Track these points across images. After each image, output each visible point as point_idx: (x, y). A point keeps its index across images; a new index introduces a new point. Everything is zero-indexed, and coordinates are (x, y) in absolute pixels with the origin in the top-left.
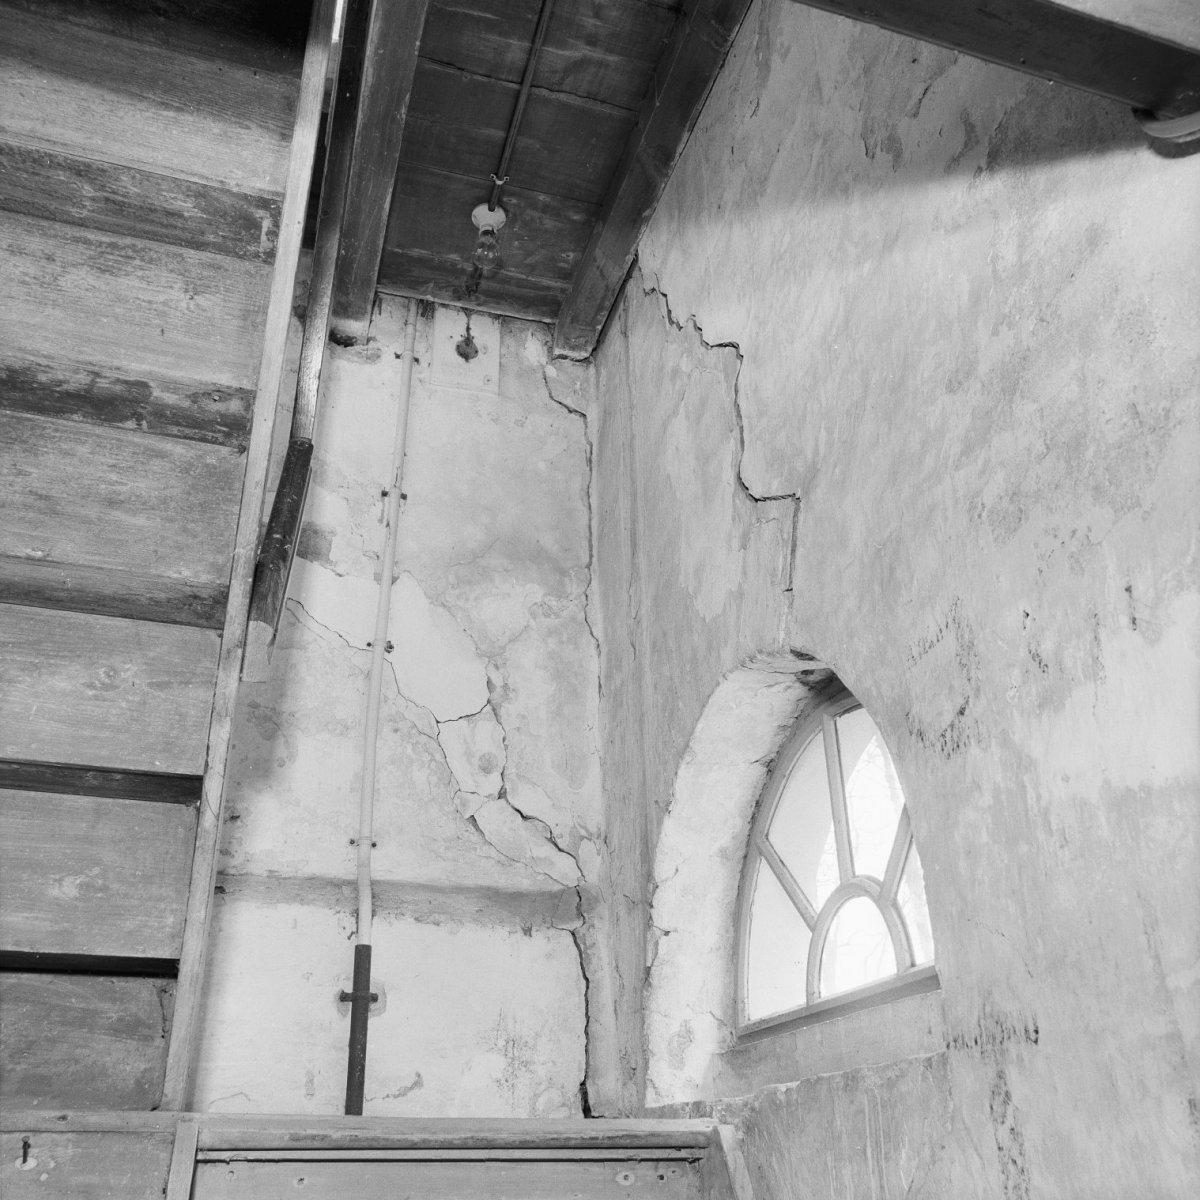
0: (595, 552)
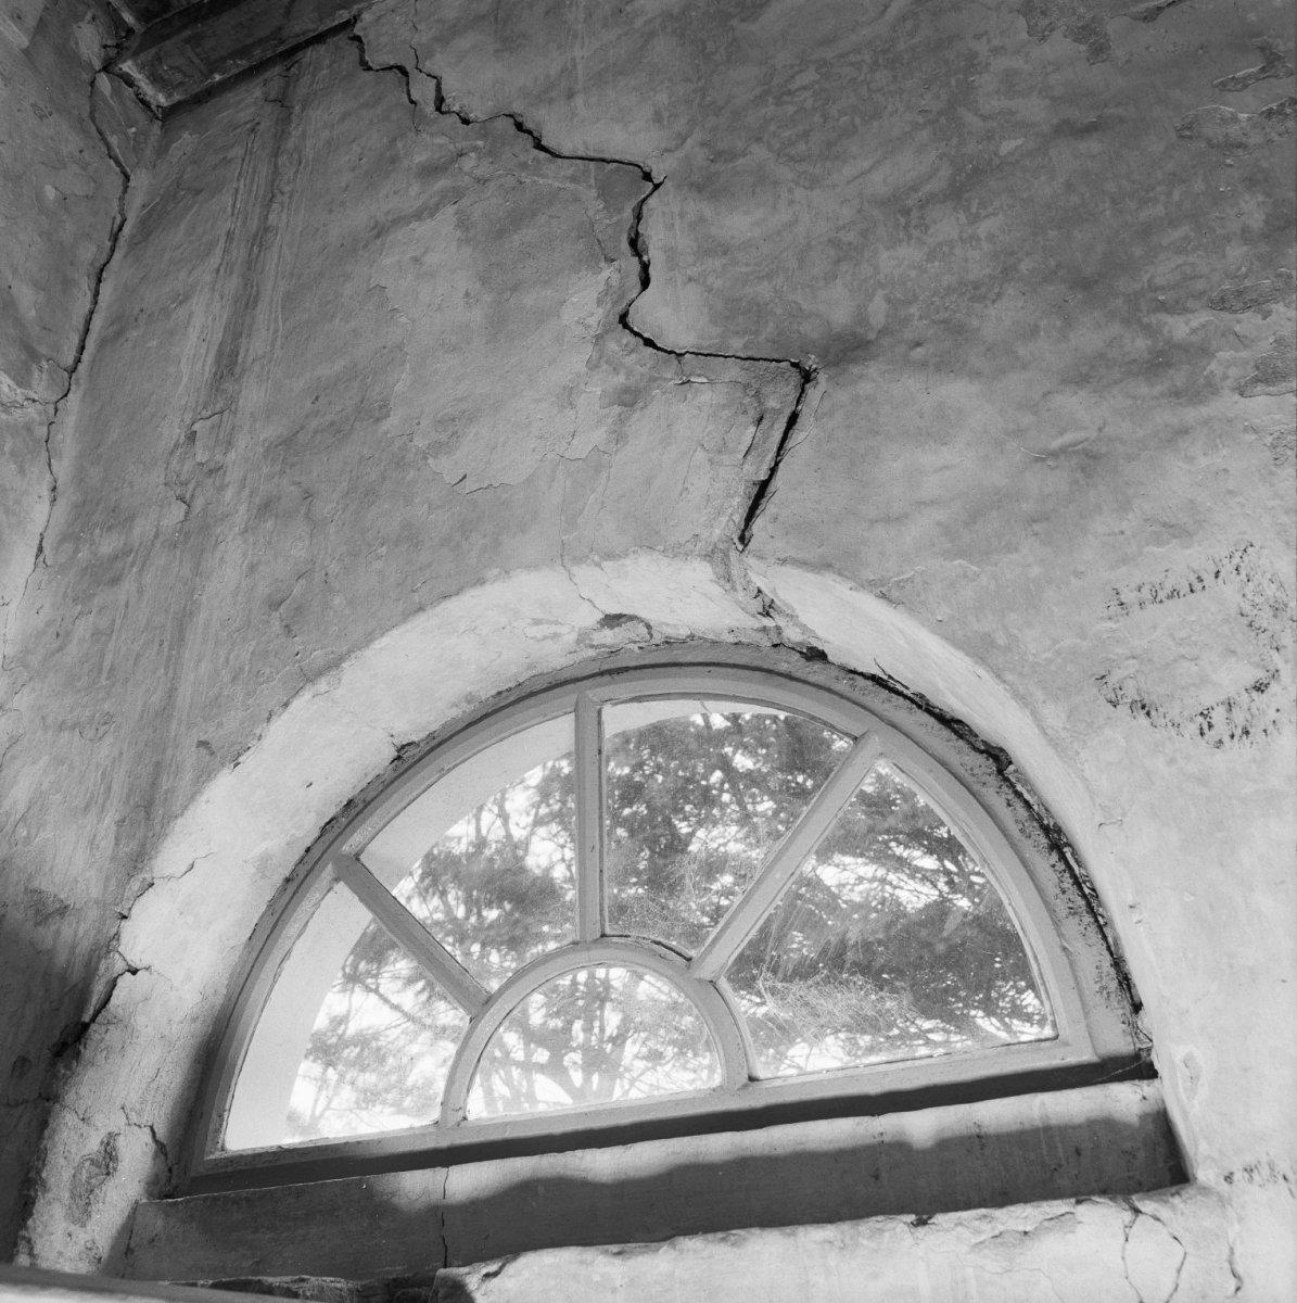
0: (86, 357)
